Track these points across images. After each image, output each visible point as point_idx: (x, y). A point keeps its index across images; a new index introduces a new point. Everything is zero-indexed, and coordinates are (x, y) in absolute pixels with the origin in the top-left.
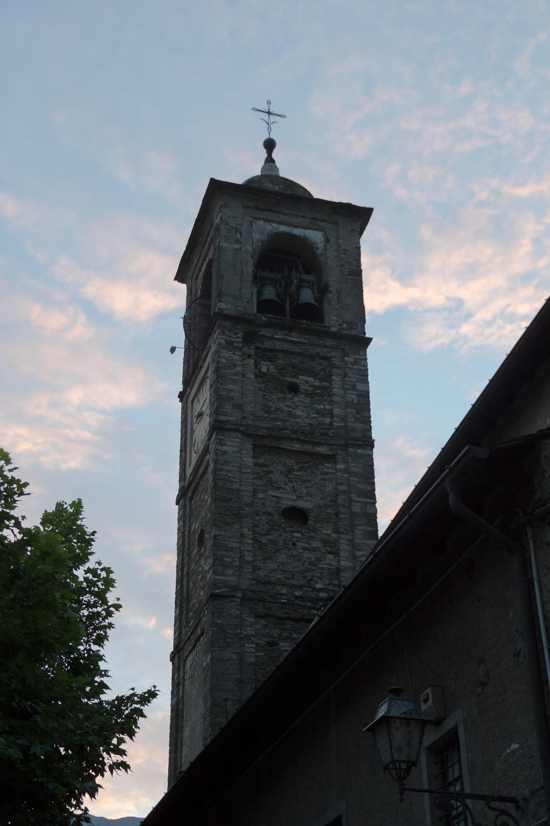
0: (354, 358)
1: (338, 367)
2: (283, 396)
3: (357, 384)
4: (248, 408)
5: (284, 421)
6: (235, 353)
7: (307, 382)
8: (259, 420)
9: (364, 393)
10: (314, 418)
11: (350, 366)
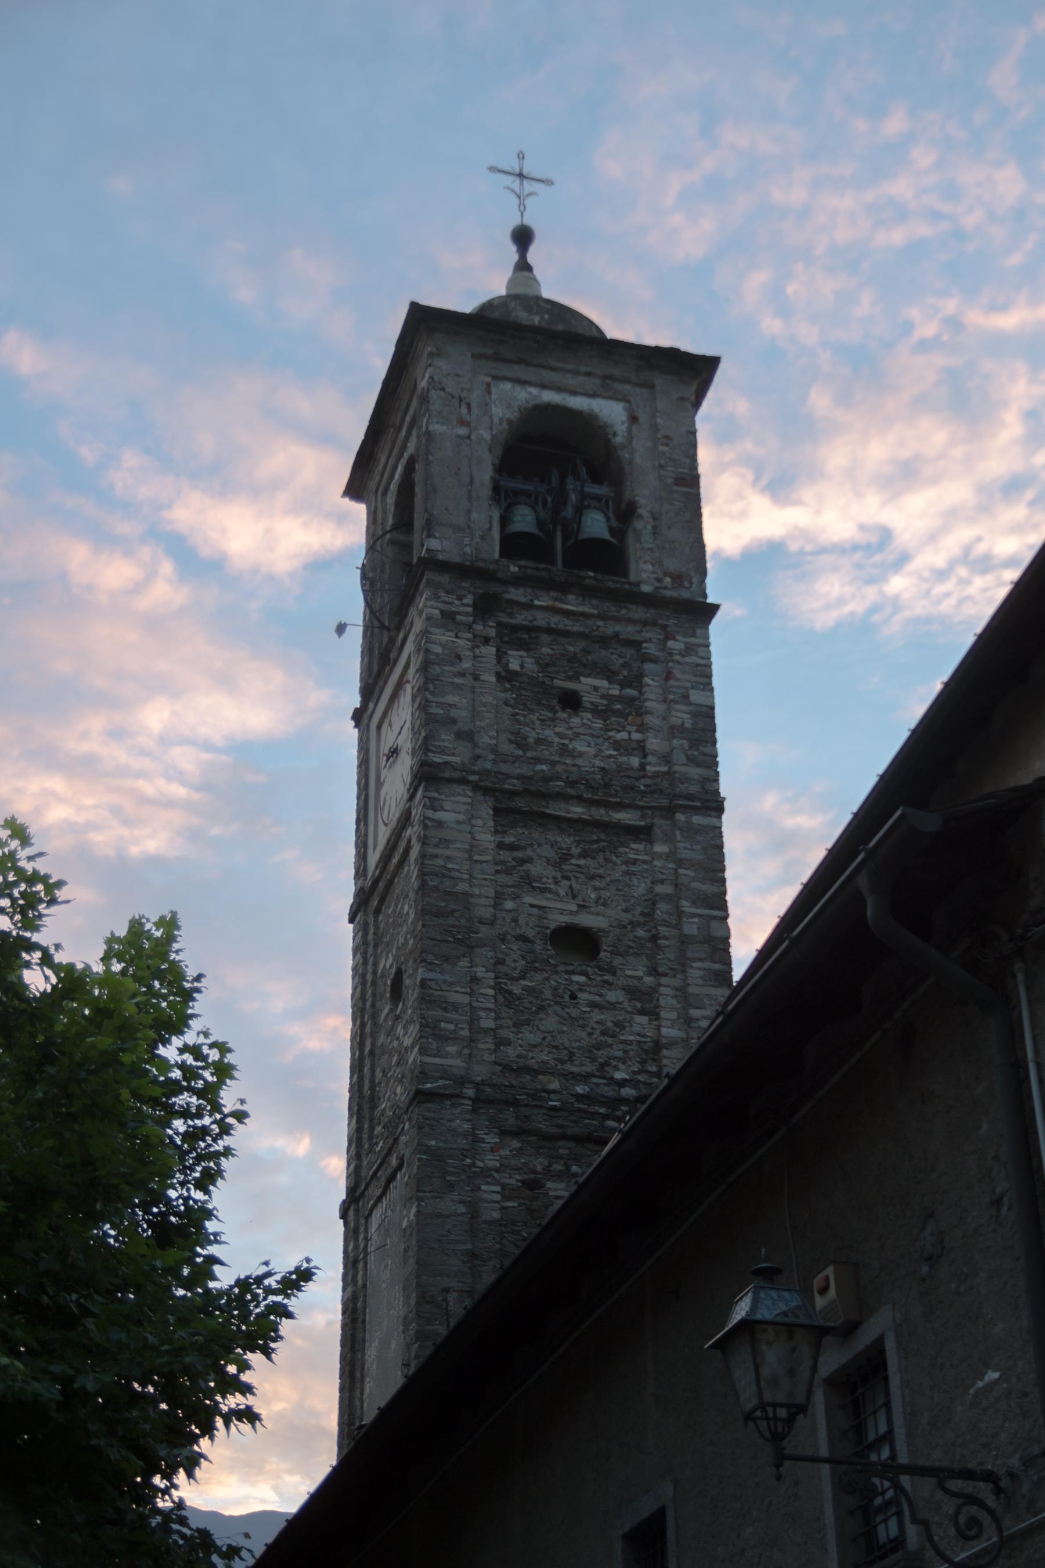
0: (685, 643)
1: (654, 660)
2: (551, 715)
3: (692, 692)
4: (485, 739)
5: (553, 764)
6: (460, 634)
7: (596, 689)
9: (704, 709)
10: (611, 756)
11: (677, 657)
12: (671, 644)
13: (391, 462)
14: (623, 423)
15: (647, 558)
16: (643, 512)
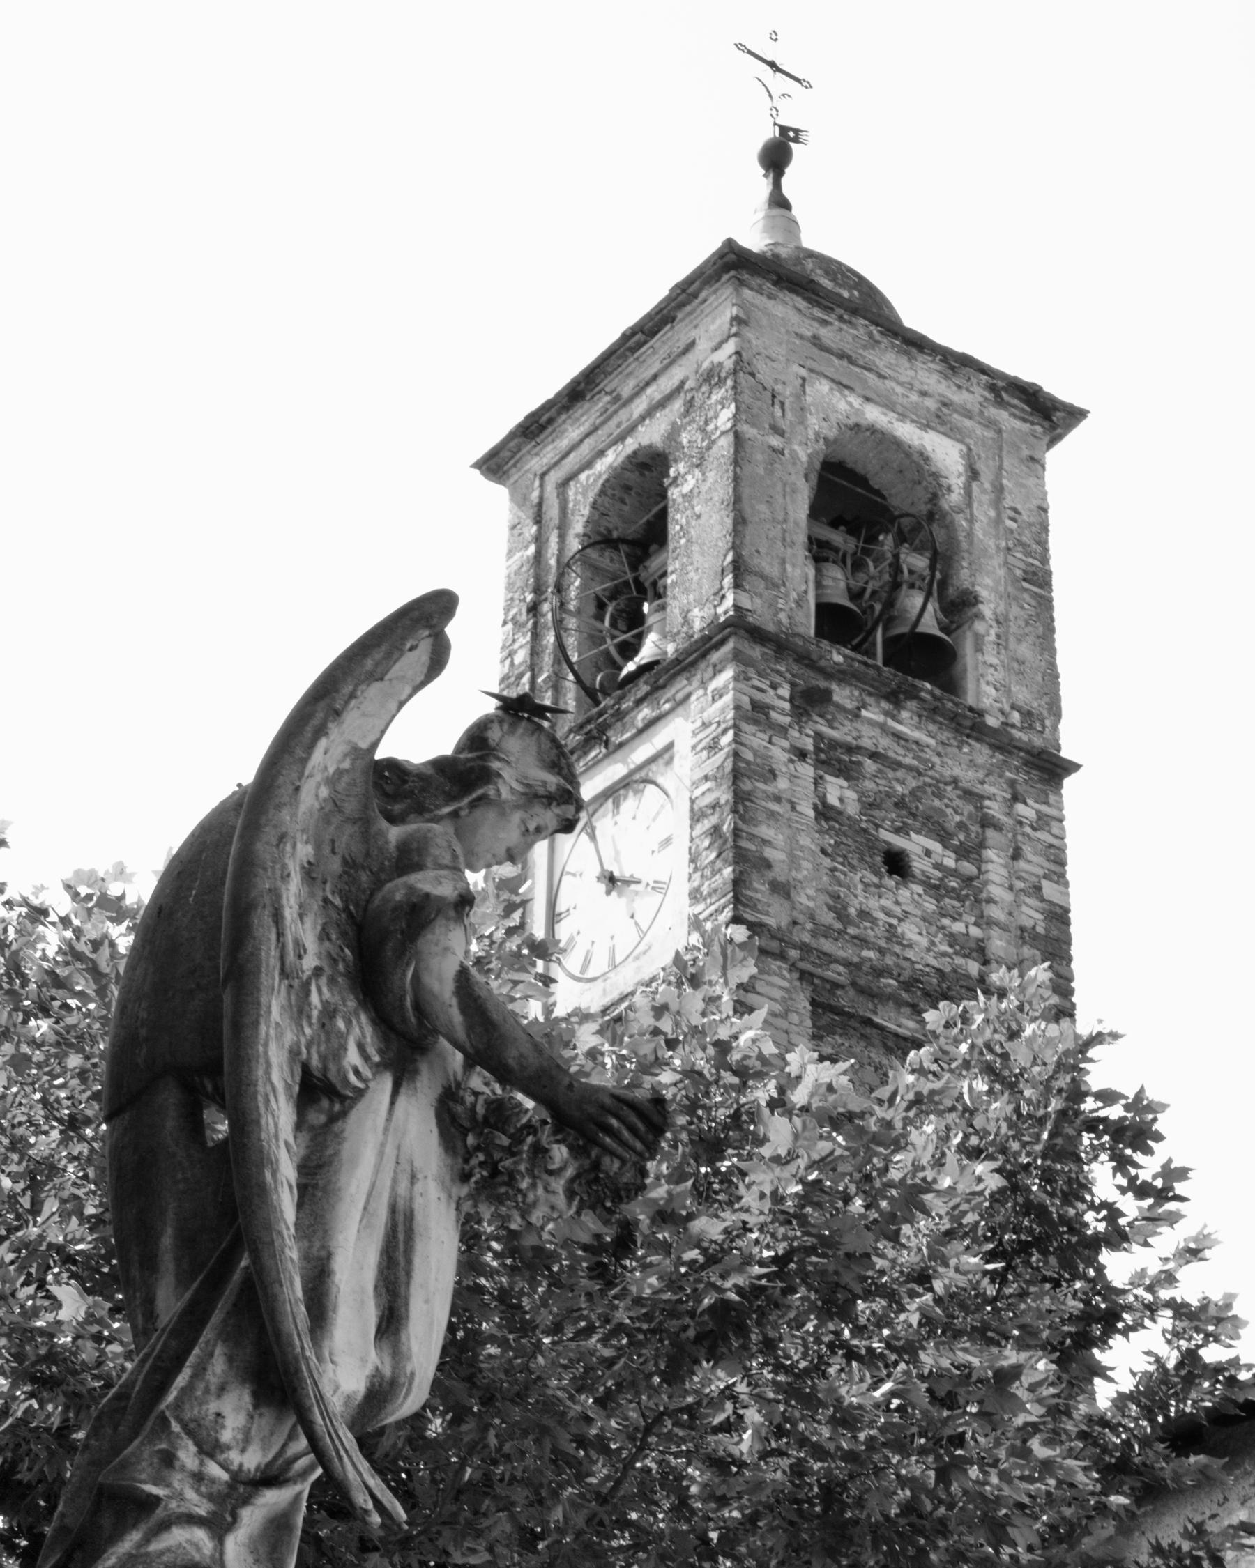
0: (1038, 812)
1: (998, 827)
2: (875, 880)
3: (1045, 883)
4: (802, 899)
5: (881, 951)
6: (775, 739)
7: (928, 853)
8: (826, 937)
9: (1059, 911)
10: (944, 954)
11: (1028, 830)
12: (1020, 808)
13: (585, 450)
14: (960, 475)
15: (990, 678)
16: (987, 610)
